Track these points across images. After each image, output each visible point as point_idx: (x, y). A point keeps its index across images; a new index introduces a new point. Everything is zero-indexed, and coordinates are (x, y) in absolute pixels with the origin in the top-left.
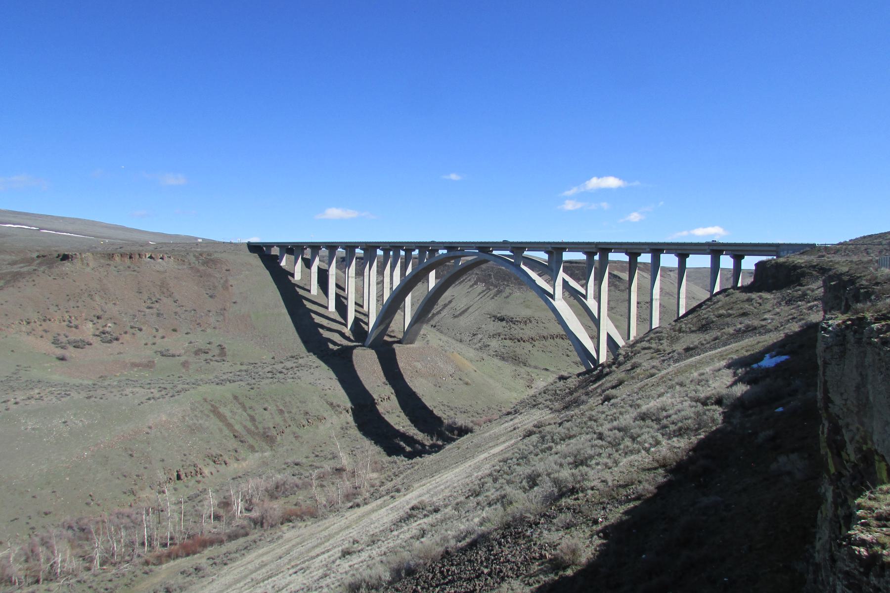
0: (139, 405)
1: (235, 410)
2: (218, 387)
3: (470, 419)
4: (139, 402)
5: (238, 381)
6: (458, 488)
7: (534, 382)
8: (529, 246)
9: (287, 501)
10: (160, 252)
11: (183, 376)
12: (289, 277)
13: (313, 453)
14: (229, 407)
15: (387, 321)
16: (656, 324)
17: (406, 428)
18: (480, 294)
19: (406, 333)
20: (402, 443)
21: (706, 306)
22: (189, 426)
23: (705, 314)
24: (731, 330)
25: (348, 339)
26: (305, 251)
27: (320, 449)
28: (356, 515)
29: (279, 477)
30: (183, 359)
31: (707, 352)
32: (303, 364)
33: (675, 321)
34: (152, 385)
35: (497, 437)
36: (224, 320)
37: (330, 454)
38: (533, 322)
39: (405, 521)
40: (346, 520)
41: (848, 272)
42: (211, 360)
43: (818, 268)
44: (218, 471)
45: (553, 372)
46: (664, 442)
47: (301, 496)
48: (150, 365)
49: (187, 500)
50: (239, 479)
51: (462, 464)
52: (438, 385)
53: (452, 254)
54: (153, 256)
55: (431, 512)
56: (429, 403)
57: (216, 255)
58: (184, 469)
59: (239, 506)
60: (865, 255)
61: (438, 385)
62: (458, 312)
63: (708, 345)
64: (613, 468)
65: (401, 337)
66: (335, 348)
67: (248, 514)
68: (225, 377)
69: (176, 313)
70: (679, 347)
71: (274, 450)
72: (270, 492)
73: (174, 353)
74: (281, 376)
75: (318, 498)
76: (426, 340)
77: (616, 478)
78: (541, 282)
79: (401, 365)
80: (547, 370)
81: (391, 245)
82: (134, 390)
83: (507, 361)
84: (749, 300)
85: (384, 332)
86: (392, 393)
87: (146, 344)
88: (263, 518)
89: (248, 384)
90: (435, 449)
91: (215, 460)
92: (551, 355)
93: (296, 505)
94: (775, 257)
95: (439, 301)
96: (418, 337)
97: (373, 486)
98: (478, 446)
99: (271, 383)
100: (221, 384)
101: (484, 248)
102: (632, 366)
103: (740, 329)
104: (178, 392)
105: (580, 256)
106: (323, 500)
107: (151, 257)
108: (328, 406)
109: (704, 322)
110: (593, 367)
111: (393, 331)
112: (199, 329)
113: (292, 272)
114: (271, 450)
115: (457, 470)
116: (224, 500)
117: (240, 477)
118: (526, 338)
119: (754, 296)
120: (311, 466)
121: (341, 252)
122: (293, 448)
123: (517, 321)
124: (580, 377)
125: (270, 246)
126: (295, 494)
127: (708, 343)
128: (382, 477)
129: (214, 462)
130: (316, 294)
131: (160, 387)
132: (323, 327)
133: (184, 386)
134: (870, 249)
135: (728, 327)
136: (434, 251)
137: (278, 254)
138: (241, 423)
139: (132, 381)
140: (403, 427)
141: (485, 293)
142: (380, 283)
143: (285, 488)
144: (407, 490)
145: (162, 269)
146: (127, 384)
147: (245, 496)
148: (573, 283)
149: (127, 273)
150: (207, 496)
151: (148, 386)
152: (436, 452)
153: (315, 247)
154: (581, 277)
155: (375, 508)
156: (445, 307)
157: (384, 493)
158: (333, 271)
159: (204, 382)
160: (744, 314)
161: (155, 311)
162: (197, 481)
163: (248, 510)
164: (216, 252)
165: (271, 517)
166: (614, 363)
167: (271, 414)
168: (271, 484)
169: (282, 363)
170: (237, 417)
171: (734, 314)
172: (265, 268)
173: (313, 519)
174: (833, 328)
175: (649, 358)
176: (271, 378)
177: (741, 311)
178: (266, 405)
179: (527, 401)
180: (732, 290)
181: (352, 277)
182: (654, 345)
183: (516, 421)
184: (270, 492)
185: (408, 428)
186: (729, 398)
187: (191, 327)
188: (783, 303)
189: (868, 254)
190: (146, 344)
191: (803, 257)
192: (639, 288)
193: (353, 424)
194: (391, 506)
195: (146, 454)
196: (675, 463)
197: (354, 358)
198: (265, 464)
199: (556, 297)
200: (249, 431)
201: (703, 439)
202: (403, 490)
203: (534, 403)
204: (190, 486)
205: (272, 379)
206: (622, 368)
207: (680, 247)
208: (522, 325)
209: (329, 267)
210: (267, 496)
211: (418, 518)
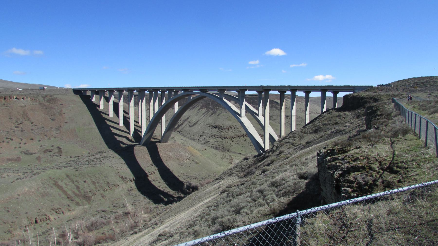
0: (12, 182)
1: (68, 183)
2: (58, 171)
3: (199, 182)
4: (12, 181)
5: (69, 167)
6: (184, 223)
7: (233, 160)
9: (97, 232)
10: (22, 95)
11: (38, 165)
13: (112, 205)
14: (64, 182)
15: (152, 131)
16: (294, 129)
17: (164, 189)
18: (204, 114)
19: (163, 137)
20: (162, 196)
21: (319, 119)
22: (41, 193)
23: (317, 124)
24: (329, 132)
26: (106, 93)
28: (133, 239)
29: (93, 219)
30: (37, 155)
33: (303, 127)
34: (20, 171)
35: (210, 192)
36: (60, 133)
37: (122, 205)
38: (233, 128)
39: (155, 242)
40: (128, 242)
41: (376, 105)
42: (53, 155)
43: (373, 99)
44: (59, 217)
45: (243, 155)
46: (277, 199)
47: (105, 229)
48: (18, 159)
49: (41, 234)
50: (71, 221)
51: (191, 208)
52: (181, 165)
53: (186, 93)
54: (18, 97)
55: (169, 237)
56: (176, 174)
57: (55, 96)
58: (39, 217)
59: (70, 237)
60: (396, 91)
61: (181, 165)
62: (192, 124)
63: (318, 141)
64: (250, 215)
65: (160, 139)
66: (124, 146)
67: (76, 240)
68: (61, 165)
69: (32, 130)
70: (303, 142)
71: (90, 204)
72: (88, 227)
73: (32, 152)
74: (94, 163)
75: (115, 229)
76: (174, 140)
77: (250, 220)
79: (161, 154)
80: (240, 154)
81: (153, 89)
82: (9, 174)
83: (219, 150)
84: (339, 116)
85: (151, 137)
86: (156, 170)
87: (15, 148)
88: (84, 242)
89: (75, 168)
90: (180, 199)
91: (57, 211)
92: (242, 145)
93: (103, 234)
94: (353, 92)
95: (182, 118)
96: (170, 139)
97: (145, 221)
98: (200, 198)
100: (59, 169)
101: (203, 90)
102: (279, 152)
103: (333, 131)
104: (34, 174)
105: (255, 93)
106: (117, 230)
107: (17, 98)
109: (317, 128)
110: (262, 152)
111: (156, 136)
112: (46, 138)
113: (99, 105)
114: (89, 204)
115: (187, 212)
116: (62, 233)
117: (71, 220)
118: (229, 137)
119: (342, 113)
120: (111, 212)
121: (125, 93)
124: (255, 158)
125: (86, 90)
126: (102, 228)
127: (317, 139)
128: (151, 216)
129: (56, 212)
130: (112, 117)
131: (24, 172)
133: (38, 170)
134: (399, 88)
135: (328, 130)
136: (176, 92)
137: (90, 95)
138: (71, 190)
139: (7, 169)
140: (162, 188)
141: (207, 113)
142: (148, 109)
143: (97, 225)
144: (161, 224)
145: (23, 105)
146: (4, 171)
147: (74, 231)
148: (251, 108)
149: (3, 108)
150: (52, 232)
151: (17, 172)
152: (179, 201)
153: (111, 91)
155: (144, 234)
157: (150, 225)
158: (121, 103)
159: (50, 168)
160: (336, 124)
161: (20, 129)
162: (47, 224)
163: (76, 238)
164: (55, 94)
165: (89, 241)
166: (271, 151)
167: (88, 184)
168: (89, 223)
170: (69, 187)
171: (331, 123)
172: (83, 103)
173: (112, 241)
174: (322, 154)
175: (288, 148)
176: (88, 164)
177: (335, 122)
178: (85, 180)
179: (227, 172)
180: (331, 110)
181: (132, 107)
182: (291, 141)
183: (220, 183)
184: (88, 227)
185: (165, 188)
186: (310, 175)
187: (42, 137)
188: (355, 117)
189: (398, 91)
190: (15, 148)
191: (366, 93)
192: (286, 108)
193: (135, 187)
194: (151, 233)
195: (17, 210)
196: (278, 212)
198: (85, 212)
199: (242, 115)
200: (76, 194)
201: (295, 197)
202: (159, 224)
203: (230, 173)
204: (42, 227)
205: (88, 165)
206: (275, 153)
207: (305, 88)
208: (227, 130)
209: (119, 101)
210: (86, 230)
211: (162, 240)
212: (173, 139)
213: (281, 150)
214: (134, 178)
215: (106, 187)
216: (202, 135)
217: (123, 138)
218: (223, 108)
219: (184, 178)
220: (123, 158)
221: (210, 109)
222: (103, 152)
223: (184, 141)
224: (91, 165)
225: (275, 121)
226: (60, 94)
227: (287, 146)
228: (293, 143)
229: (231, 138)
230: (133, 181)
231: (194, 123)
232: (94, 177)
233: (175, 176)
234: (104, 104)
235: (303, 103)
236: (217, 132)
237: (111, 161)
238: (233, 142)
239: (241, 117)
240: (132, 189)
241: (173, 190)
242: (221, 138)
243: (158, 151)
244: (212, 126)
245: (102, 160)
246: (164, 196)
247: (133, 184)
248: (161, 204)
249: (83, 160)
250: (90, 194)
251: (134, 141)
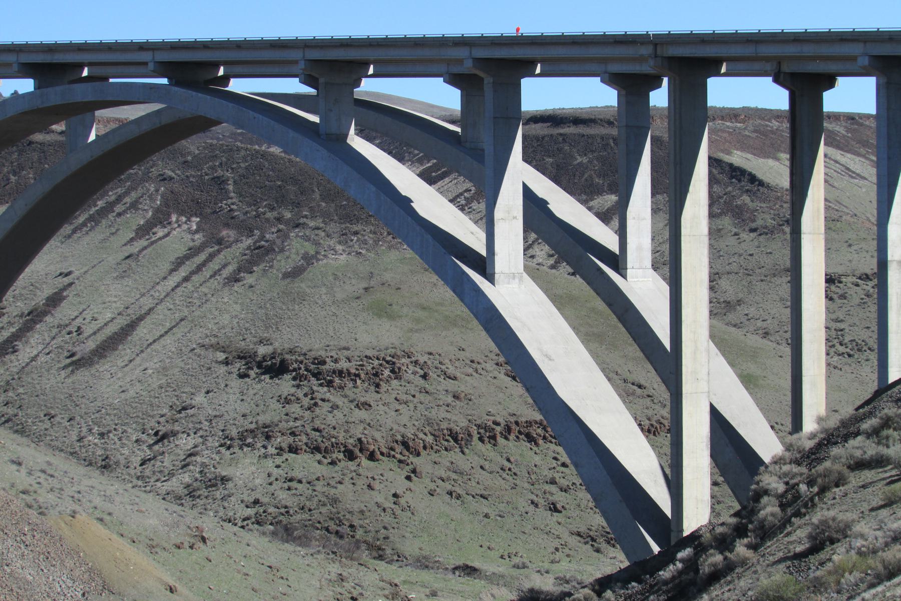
18: (179, 263)
38: (410, 372)
53: (57, 95)
62: (91, 345)
80: (469, 570)
83: (303, 541)
92: (484, 507)
102: (811, 537)
110: (656, 549)
118: (379, 439)
123: (340, 373)
141: (202, 257)
156: (34, 322)
166: (740, 531)
175: (876, 502)
199: (501, 265)
206: (776, 547)
208: (362, 391)
213: (824, 522)
216: (169, 427)
218: (327, 217)
221: (227, 225)
223: (30, 473)
225: (731, 317)
227: (864, 487)
229: (399, 448)
231: (101, 337)
236: (287, 401)
238: (418, 485)
239: (490, 278)
242: (317, 449)
244: (246, 357)
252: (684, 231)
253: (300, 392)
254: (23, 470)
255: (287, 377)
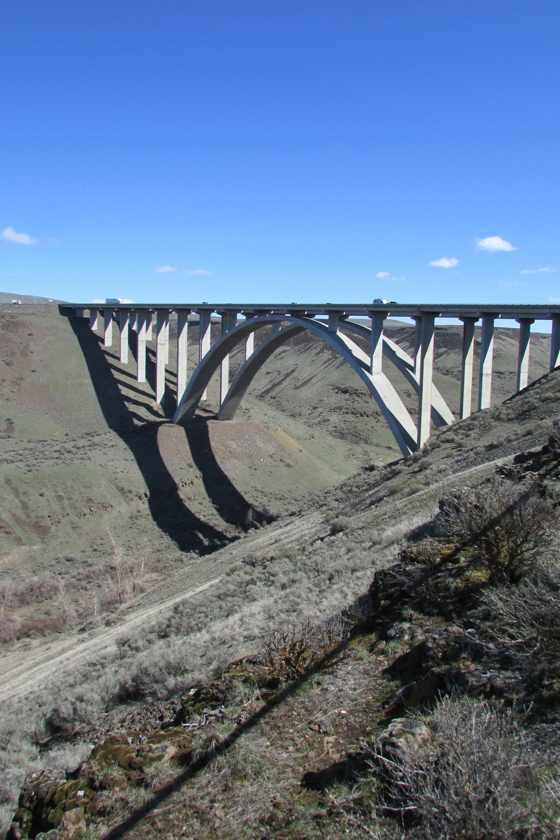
8: (392, 309)
12: (99, 343)
13: (91, 547)
17: (206, 518)
18: (325, 363)
19: (222, 407)
20: (200, 535)
25: (156, 413)
27: (99, 542)
31: (483, 462)
32: (97, 443)
52: (254, 468)
56: (239, 487)
57: (20, 318)
62: (301, 383)
66: (140, 424)
76: (248, 415)
78: (358, 353)
79: (213, 444)
80: (390, 448)
85: (195, 406)
86: (196, 477)
89: (28, 465)
99: (53, 465)
105: (410, 321)
108: (118, 492)
114: (42, 543)
118: (370, 412)
120: (84, 562)
121: (194, 316)
122: (69, 540)
123: (362, 394)
125: (81, 308)
126: (51, 598)
130: (126, 362)
132: (129, 399)
138: (10, 511)
140: (205, 516)
141: (331, 361)
143: (40, 591)
154: (441, 344)
156: (287, 377)
167: (48, 500)
169: (75, 440)
176: (57, 458)
178: (43, 490)
185: (210, 517)
197: (159, 437)
199: (374, 370)
200: (18, 521)
205: (56, 460)
212: (247, 413)
214: (148, 493)
215: (84, 509)
217: (139, 407)
219: (255, 496)
220: (132, 449)
222: (94, 434)
224: (62, 461)
226: (33, 314)
228: (460, 444)
229: (375, 414)
230: (145, 500)
231: (303, 381)
232: (64, 486)
233: (237, 491)
234: (113, 337)
235: (537, 347)
236: (347, 400)
237: (105, 454)
238: (379, 424)
239: (371, 373)
240: (139, 514)
241: (227, 521)
242: (353, 413)
243: (209, 438)
244: (338, 388)
245: (89, 452)
246: (203, 535)
247: (143, 505)
248: (192, 551)
249: (51, 449)
250: (48, 522)
251: (163, 415)
252: (424, 362)
253: (351, 398)
254: (267, 417)
255: (348, 394)
